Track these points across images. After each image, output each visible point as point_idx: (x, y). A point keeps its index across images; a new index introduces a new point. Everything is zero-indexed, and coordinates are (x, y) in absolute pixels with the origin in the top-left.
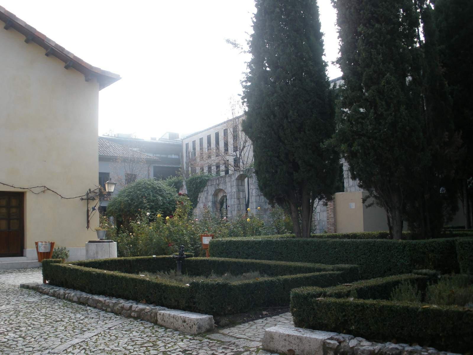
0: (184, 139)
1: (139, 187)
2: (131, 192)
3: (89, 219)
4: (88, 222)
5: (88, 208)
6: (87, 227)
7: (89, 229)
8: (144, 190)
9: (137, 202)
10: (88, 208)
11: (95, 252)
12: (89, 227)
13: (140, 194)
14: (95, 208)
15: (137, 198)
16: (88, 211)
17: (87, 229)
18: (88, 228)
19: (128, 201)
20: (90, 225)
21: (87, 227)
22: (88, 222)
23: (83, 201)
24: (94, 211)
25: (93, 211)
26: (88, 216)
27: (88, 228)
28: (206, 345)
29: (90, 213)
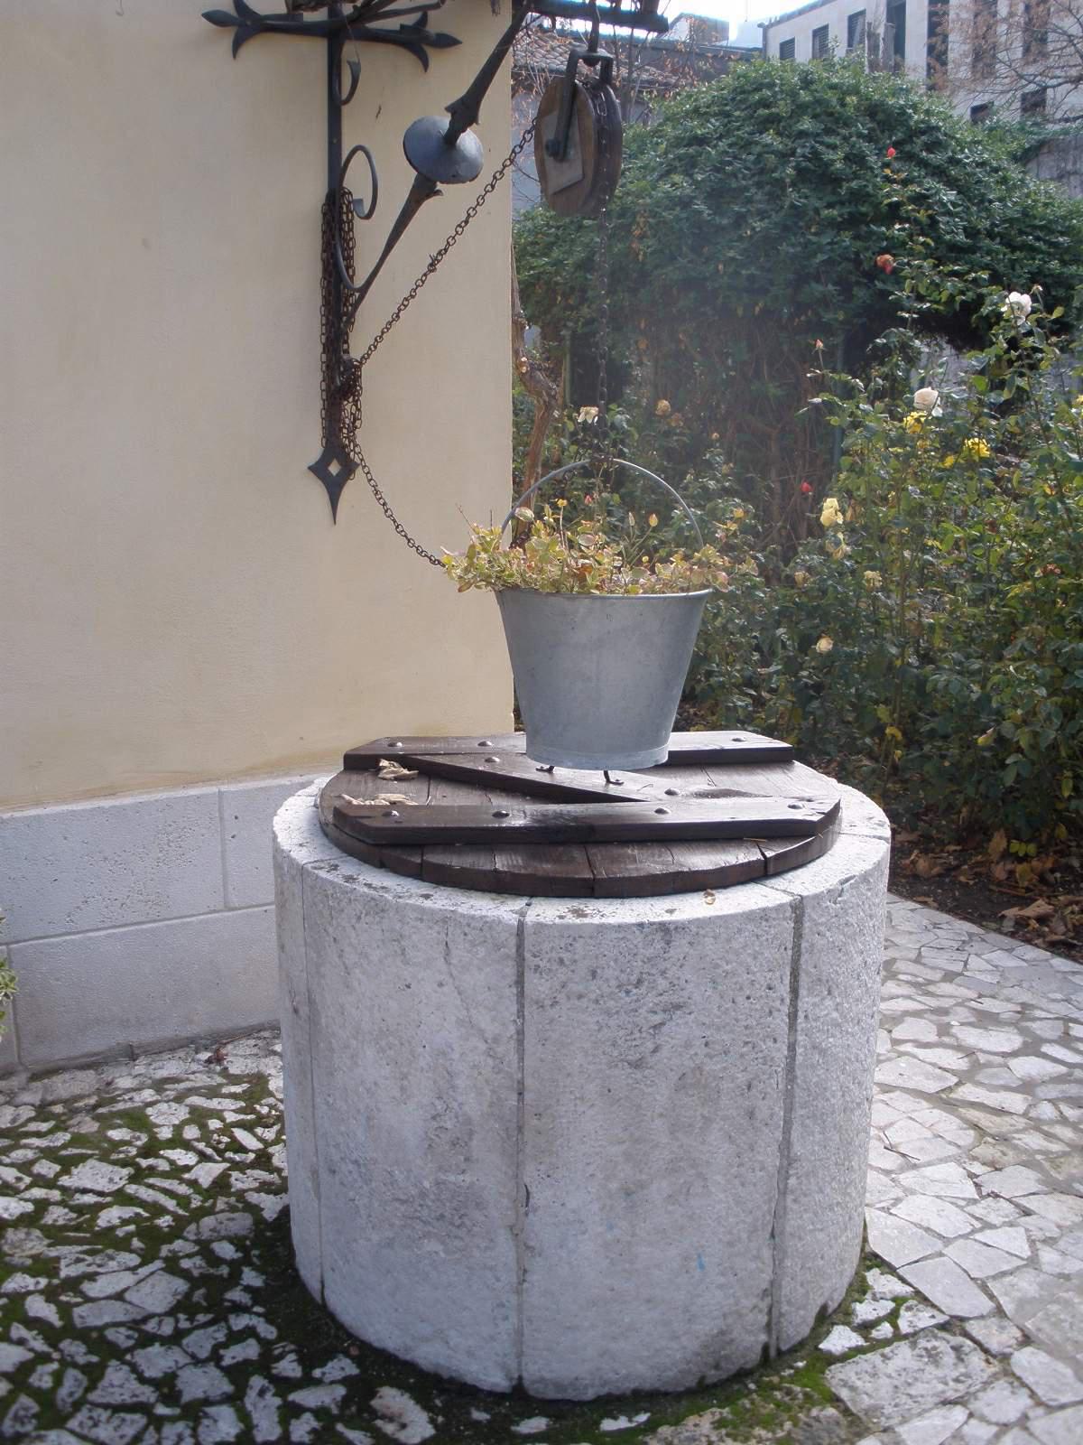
0: (771, 25)
1: (765, 104)
2: (701, 141)
3: (357, 345)
4: (341, 383)
5: (337, 169)
6: (319, 470)
7: (354, 490)
8: (806, 124)
9: (762, 215)
10: (337, 169)
11: (473, 1105)
12: (349, 469)
13: (784, 156)
14: (469, 141)
15: (759, 185)
16: (337, 214)
17: (318, 492)
18: (334, 489)
19: (685, 203)
20: (369, 441)
21: (319, 470)
22: (341, 383)
23: (260, 52)
24: (452, 198)
25: (423, 190)
26: (339, 298)
27: (334, 489)
28: (901, 977)
29: (368, 237)
